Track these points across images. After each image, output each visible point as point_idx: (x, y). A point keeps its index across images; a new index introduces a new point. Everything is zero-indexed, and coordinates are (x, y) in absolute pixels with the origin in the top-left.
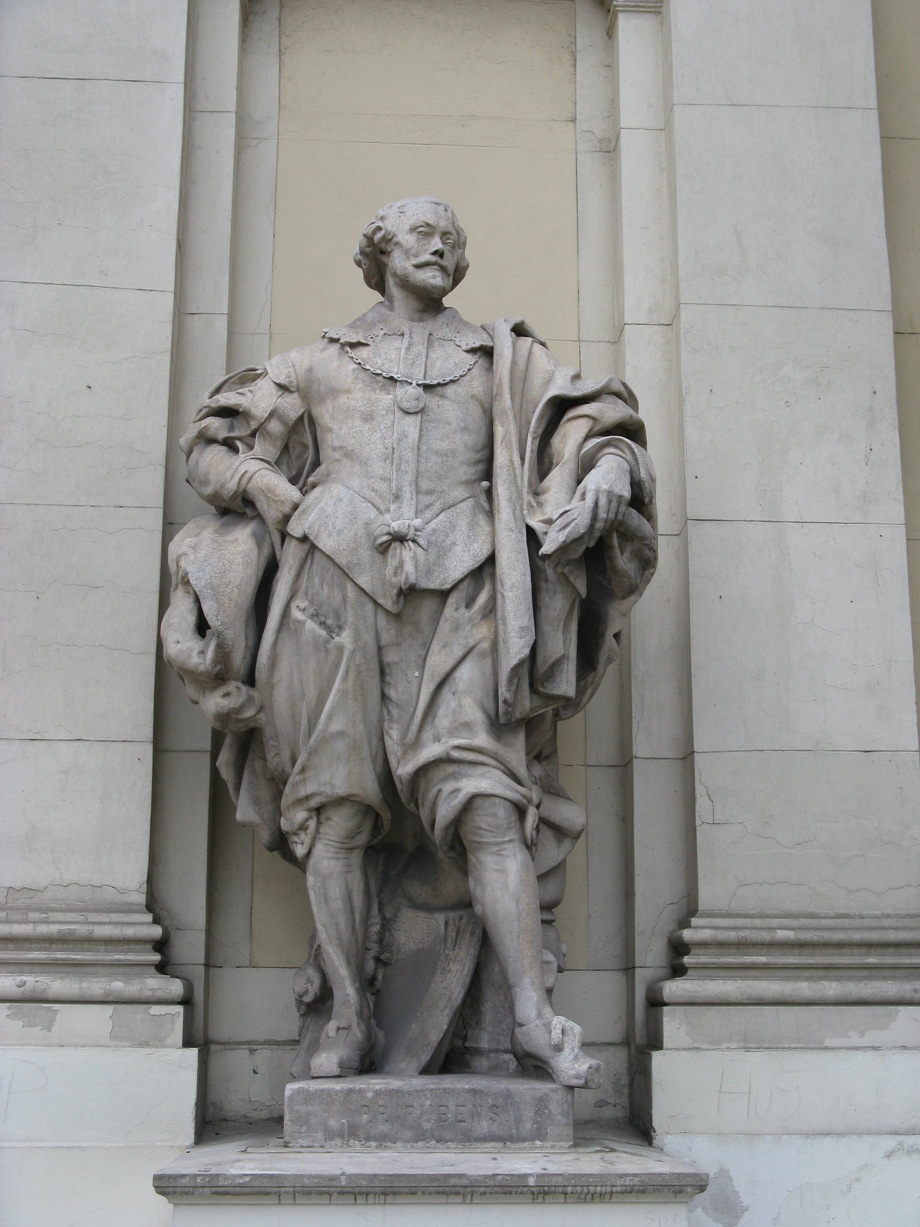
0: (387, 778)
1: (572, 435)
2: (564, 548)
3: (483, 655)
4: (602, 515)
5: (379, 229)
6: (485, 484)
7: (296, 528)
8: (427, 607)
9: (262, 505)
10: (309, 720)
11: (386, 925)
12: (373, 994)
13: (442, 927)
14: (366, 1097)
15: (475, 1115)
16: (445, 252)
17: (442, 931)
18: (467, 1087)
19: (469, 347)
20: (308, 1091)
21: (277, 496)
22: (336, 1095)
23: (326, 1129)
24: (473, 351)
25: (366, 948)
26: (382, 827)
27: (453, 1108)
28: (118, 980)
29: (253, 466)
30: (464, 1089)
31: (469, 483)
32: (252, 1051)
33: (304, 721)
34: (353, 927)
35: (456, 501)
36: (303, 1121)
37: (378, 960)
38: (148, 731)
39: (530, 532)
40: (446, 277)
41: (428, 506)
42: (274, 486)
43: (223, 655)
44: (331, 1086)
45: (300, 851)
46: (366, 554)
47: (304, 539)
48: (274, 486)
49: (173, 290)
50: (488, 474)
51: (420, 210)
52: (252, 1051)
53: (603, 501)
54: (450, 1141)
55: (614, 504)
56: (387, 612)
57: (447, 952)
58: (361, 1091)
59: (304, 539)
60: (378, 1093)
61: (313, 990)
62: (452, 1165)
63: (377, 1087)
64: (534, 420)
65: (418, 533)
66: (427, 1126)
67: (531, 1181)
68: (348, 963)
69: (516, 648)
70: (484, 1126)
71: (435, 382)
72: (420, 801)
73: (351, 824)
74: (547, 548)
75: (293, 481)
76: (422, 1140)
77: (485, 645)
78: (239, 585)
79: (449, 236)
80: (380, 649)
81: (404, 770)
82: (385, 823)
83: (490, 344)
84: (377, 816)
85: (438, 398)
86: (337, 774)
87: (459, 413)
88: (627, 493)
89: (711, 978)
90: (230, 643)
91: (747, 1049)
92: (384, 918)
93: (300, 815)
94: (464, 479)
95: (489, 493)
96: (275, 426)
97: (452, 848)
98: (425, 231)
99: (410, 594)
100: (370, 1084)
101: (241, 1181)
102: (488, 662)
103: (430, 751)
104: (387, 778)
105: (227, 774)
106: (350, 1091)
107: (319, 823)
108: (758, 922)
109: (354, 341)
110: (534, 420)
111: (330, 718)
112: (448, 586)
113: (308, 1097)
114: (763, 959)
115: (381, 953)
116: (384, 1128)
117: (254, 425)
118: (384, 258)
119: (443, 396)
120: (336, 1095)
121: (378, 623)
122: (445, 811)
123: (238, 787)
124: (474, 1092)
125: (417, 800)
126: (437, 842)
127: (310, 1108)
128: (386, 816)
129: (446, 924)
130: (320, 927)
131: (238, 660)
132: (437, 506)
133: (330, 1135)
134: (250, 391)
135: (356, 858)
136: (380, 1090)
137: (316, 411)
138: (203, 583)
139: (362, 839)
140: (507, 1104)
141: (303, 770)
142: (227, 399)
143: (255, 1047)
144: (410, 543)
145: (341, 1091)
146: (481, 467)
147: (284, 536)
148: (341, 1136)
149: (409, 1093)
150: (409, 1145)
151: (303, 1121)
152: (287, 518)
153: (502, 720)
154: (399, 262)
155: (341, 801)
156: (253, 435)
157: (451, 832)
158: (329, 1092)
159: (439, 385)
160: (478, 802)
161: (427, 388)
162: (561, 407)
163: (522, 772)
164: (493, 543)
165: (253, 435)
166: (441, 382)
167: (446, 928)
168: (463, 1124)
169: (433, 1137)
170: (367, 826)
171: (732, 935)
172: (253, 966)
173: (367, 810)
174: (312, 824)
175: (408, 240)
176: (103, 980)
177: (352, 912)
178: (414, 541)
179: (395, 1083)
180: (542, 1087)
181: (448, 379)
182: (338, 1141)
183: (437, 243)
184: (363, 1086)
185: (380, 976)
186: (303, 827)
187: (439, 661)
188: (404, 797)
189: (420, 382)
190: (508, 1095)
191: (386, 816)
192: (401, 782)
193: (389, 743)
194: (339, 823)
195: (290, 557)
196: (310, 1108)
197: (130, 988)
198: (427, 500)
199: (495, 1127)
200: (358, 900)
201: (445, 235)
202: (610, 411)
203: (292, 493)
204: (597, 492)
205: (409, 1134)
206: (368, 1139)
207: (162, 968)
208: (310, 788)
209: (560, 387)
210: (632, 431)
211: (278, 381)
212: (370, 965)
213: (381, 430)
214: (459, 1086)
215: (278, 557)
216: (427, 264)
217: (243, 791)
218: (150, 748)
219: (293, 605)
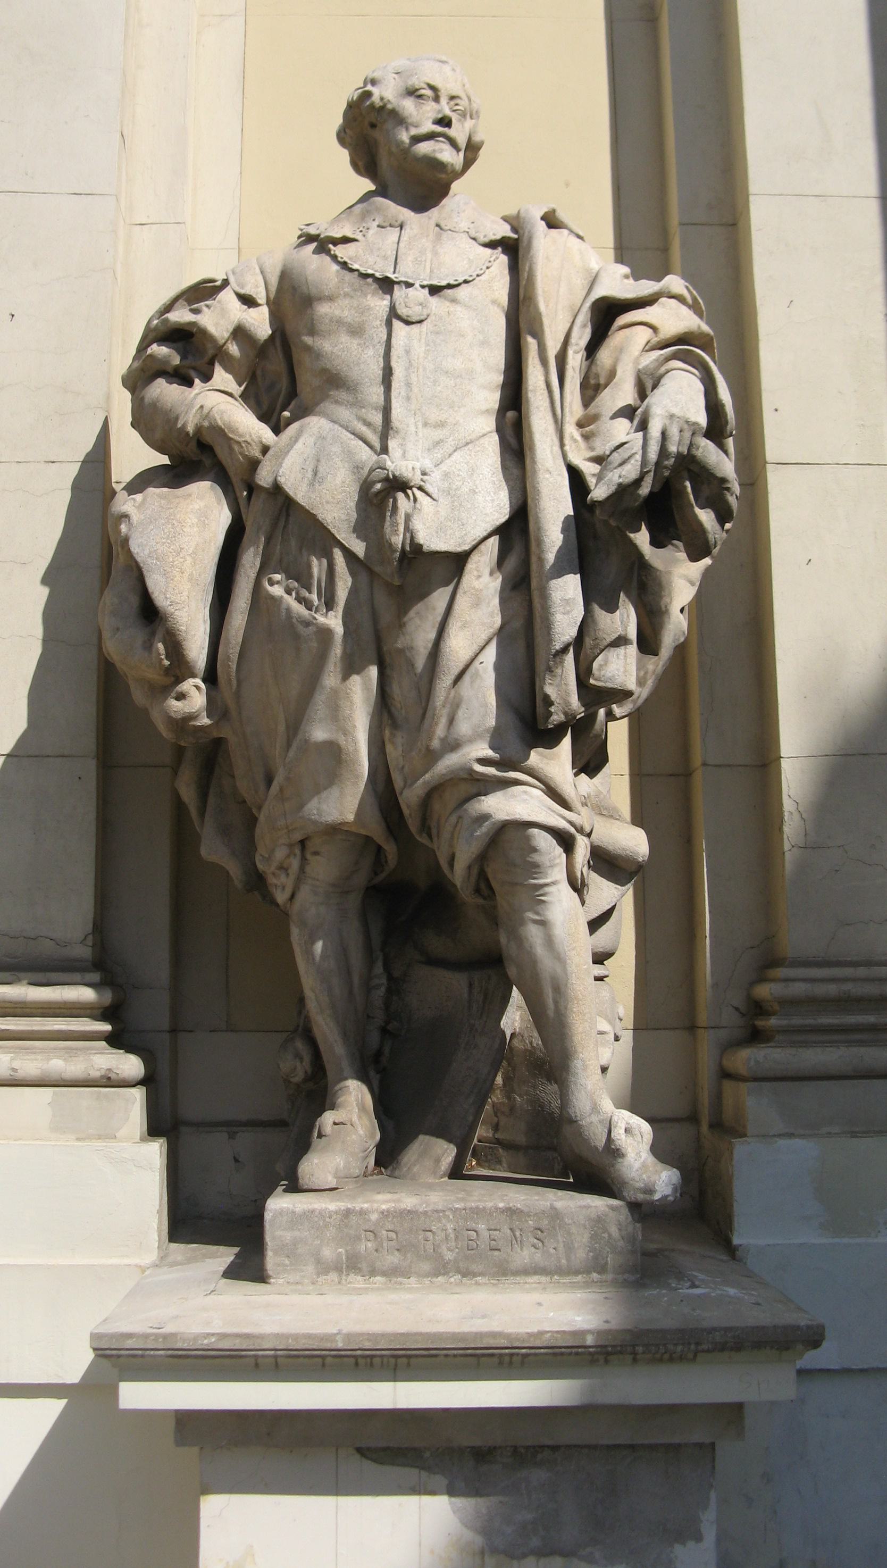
10: (288, 727)
11: (395, 986)
12: (378, 1072)
13: (466, 990)
14: (369, 1220)
15: (515, 1240)
16: (453, 120)
17: (466, 995)
18: (501, 1205)
19: (487, 240)
20: (293, 1212)
21: (241, 436)
22: (330, 1217)
23: (318, 1261)
25: (368, 1017)
26: (386, 862)
27: (485, 1234)
28: (59, 1057)
30: (497, 1208)
32: (232, 1136)
33: (282, 728)
34: (351, 992)
35: (473, 436)
36: (291, 1251)
37: (384, 1031)
38: (89, 742)
40: (455, 152)
41: (438, 443)
44: (324, 1206)
52: (232, 1136)
53: (674, 432)
54: (481, 1274)
55: (687, 435)
56: (388, 585)
57: (472, 1022)
58: (362, 1213)
60: (385, 1214)
61: (299, 1069)
62: (484, 1317)
63: (384, 1207)
65: (425, 478)
66: (449, 1256)
68: (345, 1035)
70: (525, 1255)
71: (444, 283)
72: (434, 831)
74: (599, 493)
75: (264, 417)
76: (444, 1274)
78: (194, 553)
79: (458, 101)
82: (390, 857)
85: (448, 304)
87: (475, 322)
89: (805, 1044)
90: (183, 628)
91: (854, 1135)
92: (390, 978)
94: (484, 408)
97: (477, 891)
100: (374, 1201)
101: (206, 1342)
106: (348, 1213)
108: (861, 972)
109: (338, 235)
112: (467, 547)
113: (296, 1219)
114: (871, 1019)
115: (387, 1022)
116: (393, 1259)
118: (376, 134)
119: (454, 301)
120: (330, 1217)
121: (481, 658)
123: (202, 812)
124: (511, 1212)
125: (429, 828)
126: (458, 884)
127: (297, 1233)
128: (390, 849)
129: (471, 985)
130: (308, 993)
133: (324, 1268)
134: (207, 306)
135: (354, 901)
136: (388, 1211)
138: (146, 552)
139: (361, 879)
140: (554, 1228)
142: (181, 316)
143: (235, 1129)
144: (415, 490)
145: (336, 1213)
148: (338, 1269)
149: (425, 1213)
150: (427, 1281)
151: (291, 1251)
157: (475, 871)
158: (322, 1214)
159: (449, 286)
161: (435, 290)
164: (475, 547)
166: (452, 282)
167: (470, 992)
168: (496, 1253)
169: (458, 1271)
171: (832, 989)
172: (231, 1028)
176: (39, 1057)
177: (349, 973)
178: (420, 488)
179: (408, 1201)
180: (597, 1203)
181: (461, 280)
182: (333, 1276)
184: (366, 1206)
185: (387, 1050)
186: (283, 868)
188: (413, 824)
189: (425, 283)
190: (555, 1215)
191: (390, 849)
192: (408, 807)
196: (297, 1233)
197: (73, 1068)
198: (438, 434)
199: (538, 1256)
200: (357, 959)
203: (264, 432)
205: (426, 1266)
206: (373, 1272)
207: (115, 1040)
211: (242, 292)
212: (374, 1039)
213: (374, 346)
214: (489, 1205)
215: (244, 516)
217: (207, 818)
218: (92, 764)
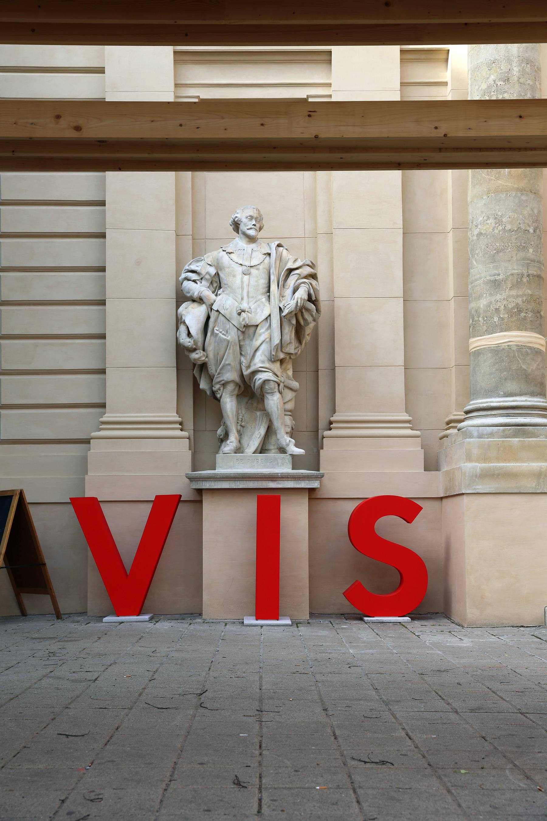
0: (242, 375)
1: (292, 281)
2: (290, 313)
3: (267, 342)
4: (299, 305)
5: (237, 217)
6: (268, 294)
7: (215, 307)
8: (252, 330)
9: (205, 300)
24: (265, 254)
29: (203, 289)
31: (263, 294)
39: (280, 308)
42: (207, 293)
43: (195, 342)
45: (218, 396)
46: (235, 314)
47: (218, 311)
48: (207, 293)
49: (396, 175)
50: (269, 291)
51: (251, 212)
53: (299, 301)
55: (302, 302)
59: (218, 311)
64: (470, 180)
67: (279, 474)
69: (276, 340)
73: (233, 388)
77: (268, 340)
80: (239, 341)
81: (246, 373)
83: (270, 252)
84: (240, 386)
86: (230, 375)
88: (306, 297)
93: (218, 386)
95: (269, 296)
96: (207, 277)
98: (251, 218)
99: (247, 326)
102: (269, 344)
103: (252, 369)
104: (242, 375)
105: (197, 376)
107: (224, 388)
110: (470, 180)
111: (226, 360)
117: (202, 276)
122: (258, 383)
128: (242, 386)
131: (200, 344)
132: (254, 301)
137: (220, 273)
139: (236, 392)
141: (219, 374)
146: (267, 289)
147: (211, 309)
152: (212, 304)
153: (272, 360)
154: (242, 227)
155: (232, 381)
156: (202, 279)
160: (266, 382)
162: (290, 271)
163: (279, 374)
165: (202, 279)
170: (237, 389)
173: (237, 384)
174: (222, 388)
175: (244, 220)
183: (254, 222)
187: (257, 343)
193: (242, 366)
194: (230, 387)
195: (213, 315)
201: (256, 219)
202: (307, 270)
203: (213, 296)
204: (298, 298)
208: (221, 379)
209: (290, 265)
210: (313, 276)
216: (251, 228)
219: (215, 329)
